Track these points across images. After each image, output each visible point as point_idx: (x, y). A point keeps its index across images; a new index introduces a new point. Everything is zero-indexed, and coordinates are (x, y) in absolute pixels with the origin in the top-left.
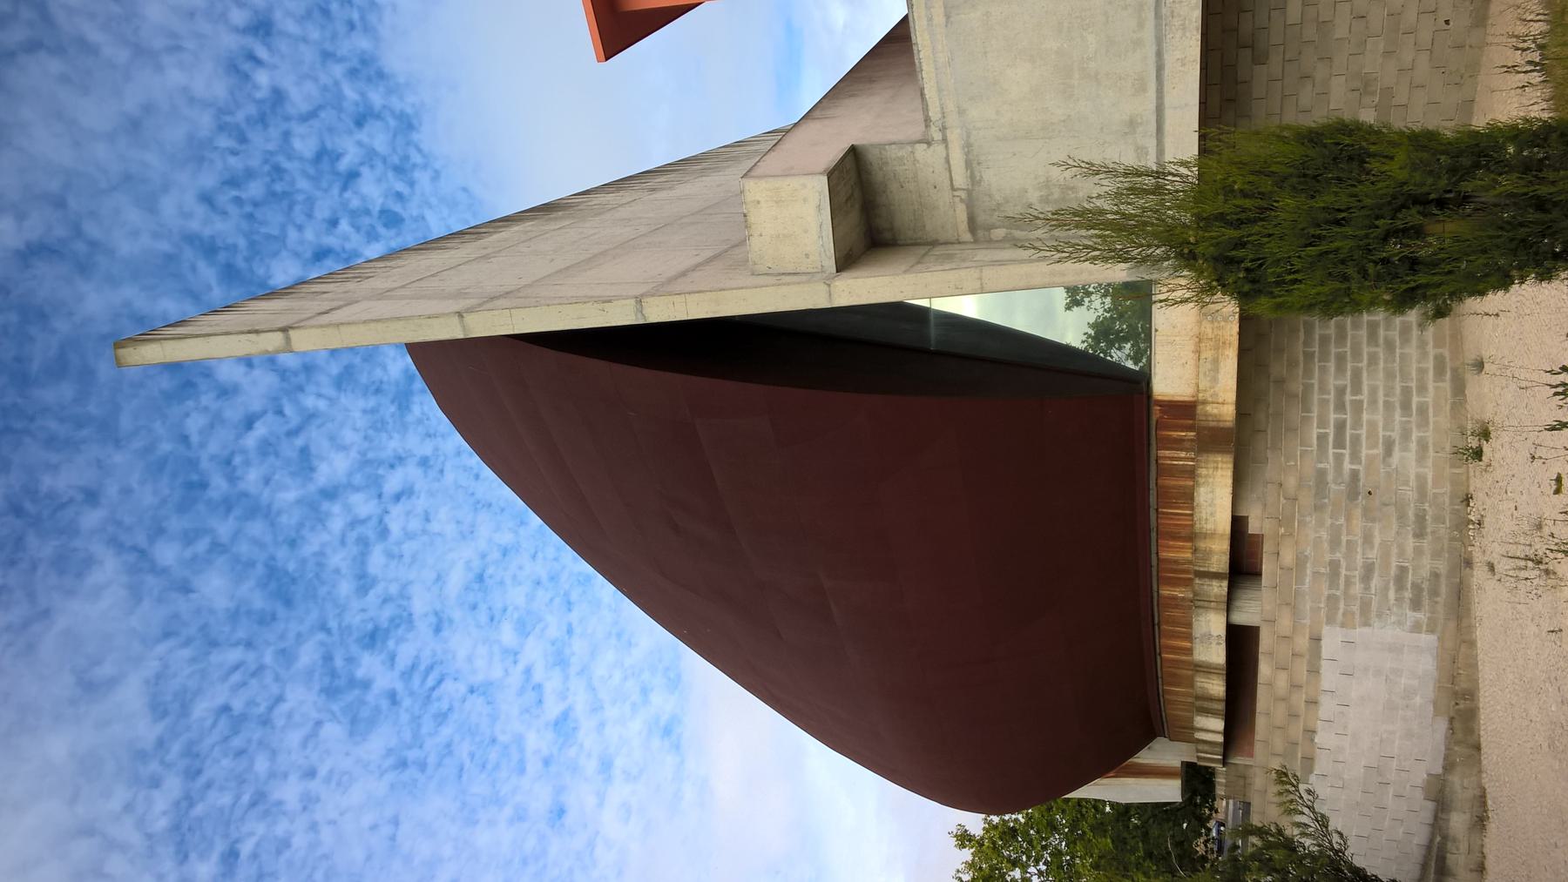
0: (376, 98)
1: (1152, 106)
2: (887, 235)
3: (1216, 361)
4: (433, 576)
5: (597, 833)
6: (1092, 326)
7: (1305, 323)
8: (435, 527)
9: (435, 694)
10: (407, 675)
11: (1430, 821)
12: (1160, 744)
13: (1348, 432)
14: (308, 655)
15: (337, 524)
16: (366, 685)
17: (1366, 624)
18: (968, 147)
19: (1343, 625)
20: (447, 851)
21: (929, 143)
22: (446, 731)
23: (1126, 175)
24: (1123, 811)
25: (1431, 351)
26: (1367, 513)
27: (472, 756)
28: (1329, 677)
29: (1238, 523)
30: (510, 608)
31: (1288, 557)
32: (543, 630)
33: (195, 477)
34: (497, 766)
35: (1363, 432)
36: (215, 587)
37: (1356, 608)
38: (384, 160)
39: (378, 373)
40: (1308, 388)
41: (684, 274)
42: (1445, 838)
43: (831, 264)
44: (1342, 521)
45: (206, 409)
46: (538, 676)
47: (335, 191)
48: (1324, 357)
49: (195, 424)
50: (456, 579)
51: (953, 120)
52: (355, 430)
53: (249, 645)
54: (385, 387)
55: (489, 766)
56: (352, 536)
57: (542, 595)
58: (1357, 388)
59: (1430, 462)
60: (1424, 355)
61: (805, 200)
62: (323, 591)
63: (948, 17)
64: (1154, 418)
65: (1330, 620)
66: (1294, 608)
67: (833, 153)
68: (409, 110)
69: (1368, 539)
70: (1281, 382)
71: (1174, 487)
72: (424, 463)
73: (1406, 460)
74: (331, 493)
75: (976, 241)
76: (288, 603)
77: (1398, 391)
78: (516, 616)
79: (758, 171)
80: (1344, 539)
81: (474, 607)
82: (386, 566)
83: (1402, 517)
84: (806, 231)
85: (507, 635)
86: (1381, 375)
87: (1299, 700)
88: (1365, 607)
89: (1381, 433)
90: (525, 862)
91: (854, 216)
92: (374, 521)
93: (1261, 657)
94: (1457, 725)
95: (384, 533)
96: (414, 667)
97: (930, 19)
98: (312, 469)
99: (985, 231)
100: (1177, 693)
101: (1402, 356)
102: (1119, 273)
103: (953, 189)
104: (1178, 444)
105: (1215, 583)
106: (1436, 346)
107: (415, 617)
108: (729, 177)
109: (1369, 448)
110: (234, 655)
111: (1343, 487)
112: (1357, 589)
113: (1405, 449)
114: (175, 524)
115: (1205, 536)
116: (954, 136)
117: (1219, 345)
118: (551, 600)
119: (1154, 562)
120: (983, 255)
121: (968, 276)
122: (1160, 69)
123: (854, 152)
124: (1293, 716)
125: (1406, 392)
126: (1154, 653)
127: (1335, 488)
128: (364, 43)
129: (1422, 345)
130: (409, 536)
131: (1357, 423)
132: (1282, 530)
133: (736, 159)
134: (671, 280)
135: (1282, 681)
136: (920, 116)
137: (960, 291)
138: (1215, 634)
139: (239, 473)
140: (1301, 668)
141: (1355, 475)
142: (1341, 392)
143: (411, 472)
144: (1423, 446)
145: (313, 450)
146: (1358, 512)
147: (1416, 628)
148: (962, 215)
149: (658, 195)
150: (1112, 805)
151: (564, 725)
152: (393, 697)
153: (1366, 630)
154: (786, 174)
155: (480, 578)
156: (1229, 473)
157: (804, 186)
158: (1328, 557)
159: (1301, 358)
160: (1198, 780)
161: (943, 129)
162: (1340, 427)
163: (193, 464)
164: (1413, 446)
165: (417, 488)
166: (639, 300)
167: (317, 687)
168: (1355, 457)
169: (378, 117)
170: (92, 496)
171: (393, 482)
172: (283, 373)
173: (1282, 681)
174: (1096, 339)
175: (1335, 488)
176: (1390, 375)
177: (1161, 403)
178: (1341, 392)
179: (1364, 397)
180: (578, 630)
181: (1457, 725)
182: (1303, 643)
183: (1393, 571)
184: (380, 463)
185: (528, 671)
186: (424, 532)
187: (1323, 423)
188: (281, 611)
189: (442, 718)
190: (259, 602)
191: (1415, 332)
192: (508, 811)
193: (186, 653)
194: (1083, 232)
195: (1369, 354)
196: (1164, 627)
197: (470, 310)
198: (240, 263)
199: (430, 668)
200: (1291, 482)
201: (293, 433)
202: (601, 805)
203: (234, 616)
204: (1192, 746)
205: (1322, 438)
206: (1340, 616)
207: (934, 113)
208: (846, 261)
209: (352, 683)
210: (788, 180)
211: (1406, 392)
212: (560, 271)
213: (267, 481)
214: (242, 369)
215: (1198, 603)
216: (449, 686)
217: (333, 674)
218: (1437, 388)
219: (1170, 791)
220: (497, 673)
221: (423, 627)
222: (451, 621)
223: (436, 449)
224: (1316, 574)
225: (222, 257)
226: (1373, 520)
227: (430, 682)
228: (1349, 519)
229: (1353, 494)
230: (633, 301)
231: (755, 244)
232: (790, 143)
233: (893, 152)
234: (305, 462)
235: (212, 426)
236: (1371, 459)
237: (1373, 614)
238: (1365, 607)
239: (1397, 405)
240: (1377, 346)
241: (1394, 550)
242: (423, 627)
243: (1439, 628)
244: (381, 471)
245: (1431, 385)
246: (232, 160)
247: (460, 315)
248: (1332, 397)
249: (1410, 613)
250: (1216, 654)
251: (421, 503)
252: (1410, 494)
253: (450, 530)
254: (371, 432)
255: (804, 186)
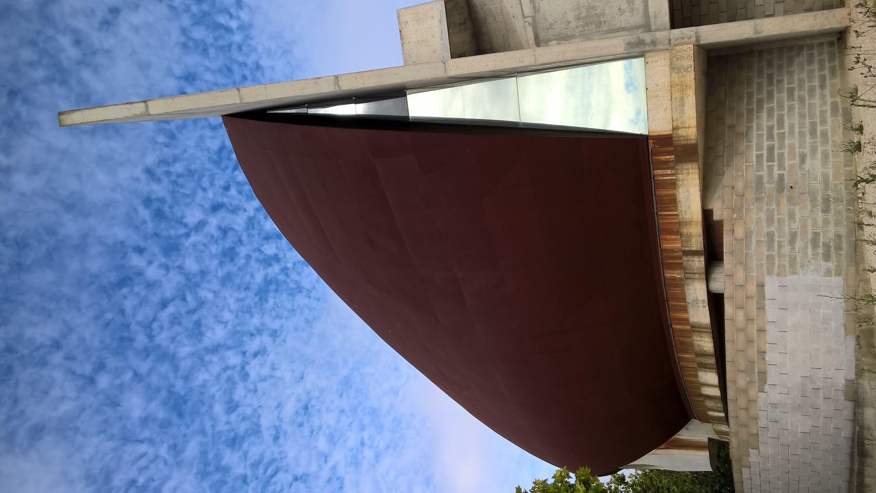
3: (682, 99)
4: (276, 404)
7: (748, 93)
8: (278, 374)
9: (274, 480)
10: (255, 465)
11: (851, 418)
12: (694, 424)
13: (776, 152)
14: (192, 450)
15: (215, 369)
16: (226, 470)
17: (794, 273)
19: (779, 275)
25: (829, 100)
26: (790, 200)
28: (772, 312)
29: (707, 214)
30: (324, 427)
31: (740, 232)
32: (345, 441)
33: (126, 334)
35: (786, 151)
36: (135, 404)
37: (786, 262)
39: (248, 278)
40: (749, 129)
42: (862, 427)
44: (774, 206)
45: (138, 294)
47: (229, 171)
48: (760, 109)
49: (129, 304)
50: (290, 408)
52: (230, 311)
53: (151, 441)
54: (252, 286)
56: (224, 376)
58: (781, 125)
59: (830, 165)
60: (824, 102)
62: (204, 409)
65: (769, 272)
66: (747, 269)
69: (792, 216)
70: (732, 127)
72: (274, 334)
73: (814, 165)
74: (215, 349)
76: (181, 415)
77: (808, 125)
80: (776, 217)
81: (301, 425)
82: (245, 396)
83: (814, 200)
85: (322, 444)
86: (797, 116)
87: (753, 329)
88: (793, 261)
89: (797, 151)
92: (239, 368)
93: (725, 300)
94: (862, 342)
95: (245, 376)
98: (201, 334)
100: (687, 360)
101: (810, 105)
103: (524, 17)
104: (665, 165)
105: (696, 259)
106: (832, 96)
107: (263, 429)
109: (789, 160)
110: (142, 448)
111: (773, 185)
112: (786, 249)
113: (814, 158)
114: (112, 362)
115: (687, 223)
117: (683, 88)
118: (351, 423)
124: (750, 341)
125: (813, 125)
127: (769, 186)
129: (823, 97)
130: (263, 379)
131: (781, 146)
132: (735, 216)
135: (740, 316)
138: (700, 299)
139: (154, 333)
140: (753, 306)
141: (781, 177)
142: (770, 129)
143: (266, 339)
144: (825, 156)
145: (204, 322)
146: (784, 201)
147: (828, 273)
152: (244, 479)
153: (794, 277)
155: (306, 408)
156: (697, 182)
158: (766, 230)
159: (745, 112)
160: (719, 450)
162: (771, 149)
163: (126, 326)
164: (819, 156)
167: (195, 471)
168: (781, 166)
170: (57, 345)
171: (253, 345)
172: (187, 276)
173: (740, 316)
175: (769, 186)
176: (802, 116)
178: (770, 129)
179: (786, 129)
181: (862, 342)
182: (752, 289)
183: (810, 236)
184: (244, 334)
185: (334, 468)
186: (272, 377)
187: (759, 148)
188: (175, 419)
190: (161, 414)
191: (818, 91)
193: (111, 444)
195: (788, 106)
196: (671, 302)
198: (166, 208)
200: (740, 185)
201: (194, 311)
203: (145, 421)
204: (708, 426)
205: (759, 157)
206: (776, 269)
209: (218, 469)
211: (813, 125)
213: (173, 339)
214: (163, 272)
215: (689, 275)
216: (281, 475)
217: (206, 464)
218: (833, 121)
219: (701, 462)
220: (313, 468)
223: (282, 326)
224: (758, 242)
225: (155, 205)
226: (795, 205)
227: (270, 471)
228: (778, 204)
229: (780, 188)
234: (197, 331)
235: (141, 304)
236: (792, 167)
237: (798, 266)
238: (793, 261)
239: (808, 133)
240: (794, 100)
241: (810, 222)
242: (267, 435)
243: (844, 272)
245: (829, 119)
246: (166, 150)
248: (765, 132)
249: (823, 263)
250: (701, 315)
251: (271, 357)
252: (818, 186)
253: (287, 376)
254: (240, 313)
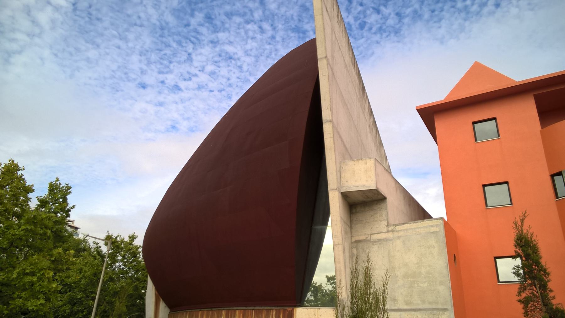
0: (406, 20)
1: (401, 307)
2: (354, 211)
5: (136, 101)
6: (321, 285)
8: (250, 41)
12: (167, 310)
18: (386, 240)
20: (130, 45)
21: (387, 226)
22: (174, 45)
23: (383, 297)
24: (142, 297)
27: (165, 54)
32: (211, 81)
34: (161, 64)
38: (384, 23)
41: (340, 137)
43: (344, 190)
46: (194, 79)
50: (230, 49)
51: (396, 234)
55: (161, 61)
57: (224, 81)
61: (367, 181)
63: (433, 233)
64: (287, 308)
67: (384, 191)
68: (402, 33)
71: (262, 315)
75: (352, 243)
78: (217, 71)
79: (377, 164)
81: (220, 55)
84: (356, 181)
85: (210, 68)
90: (126, 74)
91: (361, 198)
96: (198, 33)
97: (432, 226)
99: (355, 246)
102: (344, 295)
103: (371, 234)
108: (374, 153)
116: (390, 235)
119: (234, 308)
120: (347, 246)
121: (339, 240)
122: (414, 310)
123: (384, 199)
126: (201, 308)
128: (426, 16)
130: (246, 32)
133: (380, 156)
134: (338, 132)
136: (397, 222)
137: (334, 237)
148: (362, 238)
149: (368, 130)
150: (145, 293)
151: (176, 88)
154: (377, 175)
155: (231, 58)
157: (372, 180)
161: (392, 231)
165: (264, 35)
166: (331, 121)
169: (400, 21)
171: (266, 26)
174: (315, 287)
177: (293, 311)
180: (211, 94)
184: (273, 21)
185: (196, 75)
189: (179, 43)
192: (145, 67)
194: (363, 280)
197: (328, 61)
199: (198, 39)
202: (147, 102)
207: (398, 228)
208: (345, 196)
210: (374, 174)
212: (341, 93)
220: (196, 64)
221: (213, 37)
222: (215, 47)
230: (331, 118)
231: (351, 163)
232: (387, 175)
233: (384, 213)
244: (270, 21)
247: (326, 57)
251: (259, 36)
253: (248, 47)
255: (372, 180)
